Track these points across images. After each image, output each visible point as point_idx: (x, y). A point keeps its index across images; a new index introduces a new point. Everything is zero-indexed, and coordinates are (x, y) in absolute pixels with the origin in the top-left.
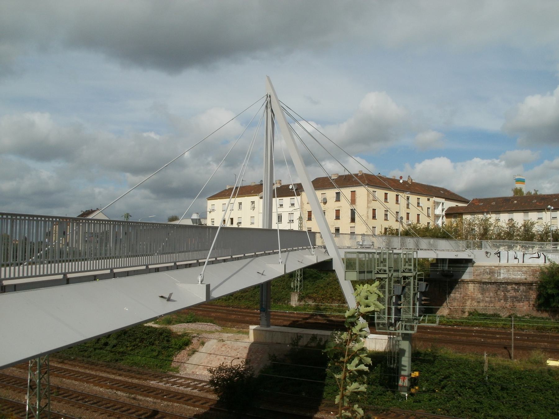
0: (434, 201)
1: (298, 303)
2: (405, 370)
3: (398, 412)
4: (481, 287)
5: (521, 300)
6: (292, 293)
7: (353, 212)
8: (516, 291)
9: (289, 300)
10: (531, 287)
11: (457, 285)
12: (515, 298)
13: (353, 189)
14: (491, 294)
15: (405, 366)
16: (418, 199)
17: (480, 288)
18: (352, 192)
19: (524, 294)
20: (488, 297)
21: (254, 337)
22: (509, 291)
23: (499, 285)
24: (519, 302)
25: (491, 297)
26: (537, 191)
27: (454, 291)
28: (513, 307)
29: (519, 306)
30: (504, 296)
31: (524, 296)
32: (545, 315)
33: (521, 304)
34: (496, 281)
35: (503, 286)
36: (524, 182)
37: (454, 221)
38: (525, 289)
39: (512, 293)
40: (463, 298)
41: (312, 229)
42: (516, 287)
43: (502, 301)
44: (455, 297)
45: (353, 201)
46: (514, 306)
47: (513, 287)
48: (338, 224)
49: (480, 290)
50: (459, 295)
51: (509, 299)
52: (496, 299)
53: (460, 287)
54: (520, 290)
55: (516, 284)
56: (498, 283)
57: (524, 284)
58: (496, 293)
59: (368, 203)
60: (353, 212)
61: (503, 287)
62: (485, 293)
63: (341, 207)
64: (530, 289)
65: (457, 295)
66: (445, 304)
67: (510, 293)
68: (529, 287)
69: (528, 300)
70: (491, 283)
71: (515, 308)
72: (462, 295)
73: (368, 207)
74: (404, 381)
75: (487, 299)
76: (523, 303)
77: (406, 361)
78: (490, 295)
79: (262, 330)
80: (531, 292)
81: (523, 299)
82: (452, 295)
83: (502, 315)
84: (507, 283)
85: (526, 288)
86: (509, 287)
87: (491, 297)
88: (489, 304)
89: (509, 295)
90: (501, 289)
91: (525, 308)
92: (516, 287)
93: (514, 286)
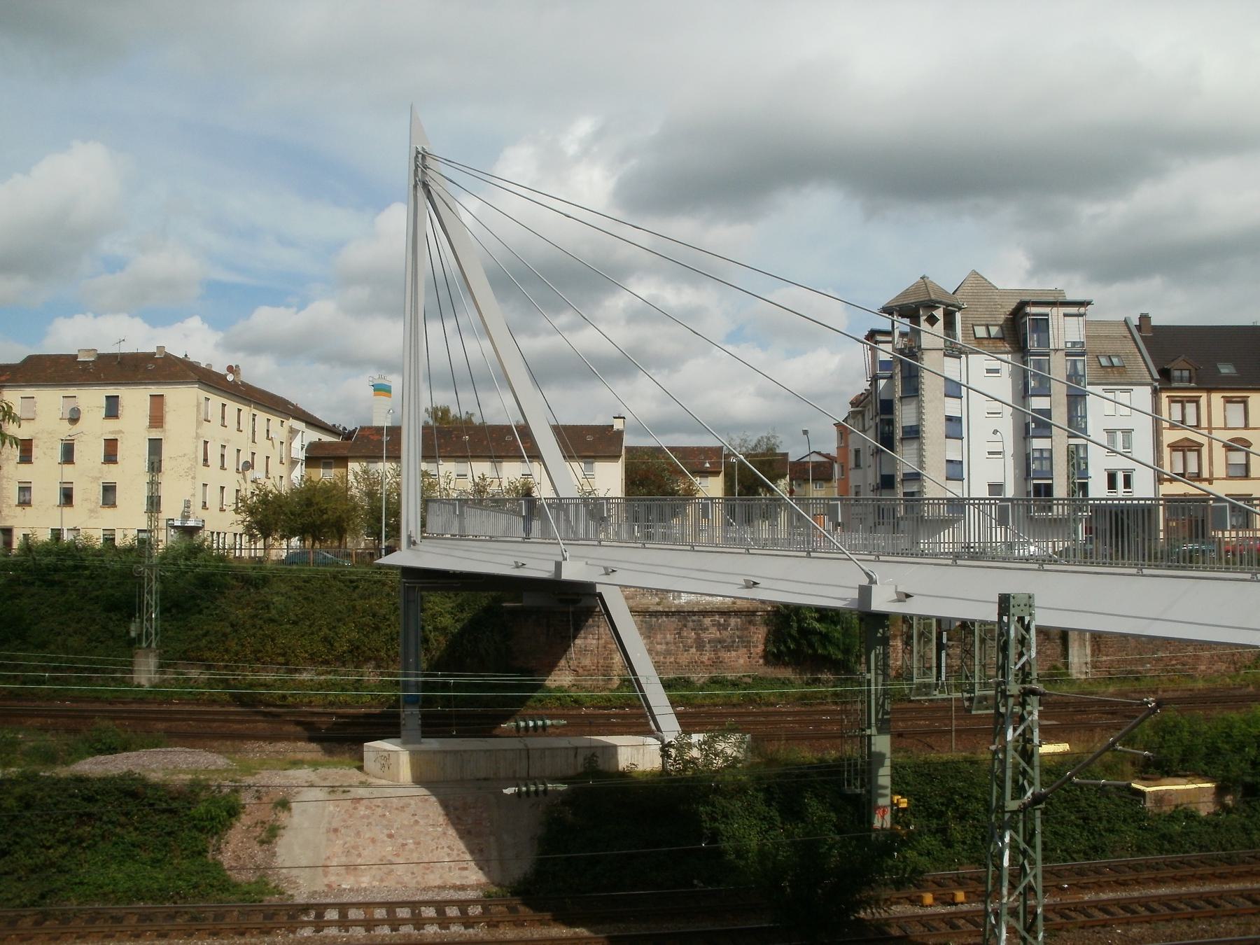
0: (291, 427)
1: (156, 678)
2: (884, 796)
3: (192, 910)
4: (646, 622)
5: (732, 646)
6: (137, 651)
7: (155, 446)
8: (723, 627)
9: (129, 667)
10: (753, 618)
11: (591, 620)
12: (720, 642)
13: (112, 391)
14: (668, 636)
15: (884, 787)
16: (268, 420)
17: (644, 625)
18: (951, 465)
19: (738, 633)
20: (661, 644)
21: (412, 770)
22: (707, 629)
23: (685, 618)
24: (729, 651)
25: (667, 644)
26: (472, 415)
27: (582, 634)
28: (716, 663)
29: (730, 658)
30: (695, 639)
31: (738, 637)
32: (787, 673)
33: (734, 654)
34: (681, 609)
35: (694, 618)
36: (389, 392)
37: (324, 475)
38: (739, 623)
39: (714, 633)
40: (605, 647)
41: (32, 485)
42: (722, 621)
43: (693, 650)
44: (586, 646)
45: (157, 419)
46: (718, 658)
47: (715, 620)
48: (111, 474)
49: (644, 629)
50: (594, 642)
51: (707, 645)
52: (679, 647)
53: (596, 623)
54: (729, 625)
55: (722, 613)
56: (684, 612)
57: (738, 613)
58: (679, 633)
59: (197, 428)
60: (155, 446)
61: (693, 621)
62: (655, 634)
63: (120, 432)
64: (750, 622)
65: (589, 641)
66: (563, 662)
67: (710, 633)
68: (748, 618)
69: (747, 644)
70: (667, 614)
71: (721, 662)
72: (601, 642)
73: (198, 437)
74: (883, 817)
75: (658, 646)
76: (737, 651)
77: (884, 777)
78: (665, 638)
79: (445, 752)
80: (752, 629)
81: (735, 645)
82: (578, 641)
83: (694, 677)
84: (705, 613)
85: (742, 621)
86: (707, 621)
87: (667, 644)
88: (665, 658)
89: (706, 636)
90: (690, 624)
91: (741, 661)
92: (722, 621)
93: (717, 618)
